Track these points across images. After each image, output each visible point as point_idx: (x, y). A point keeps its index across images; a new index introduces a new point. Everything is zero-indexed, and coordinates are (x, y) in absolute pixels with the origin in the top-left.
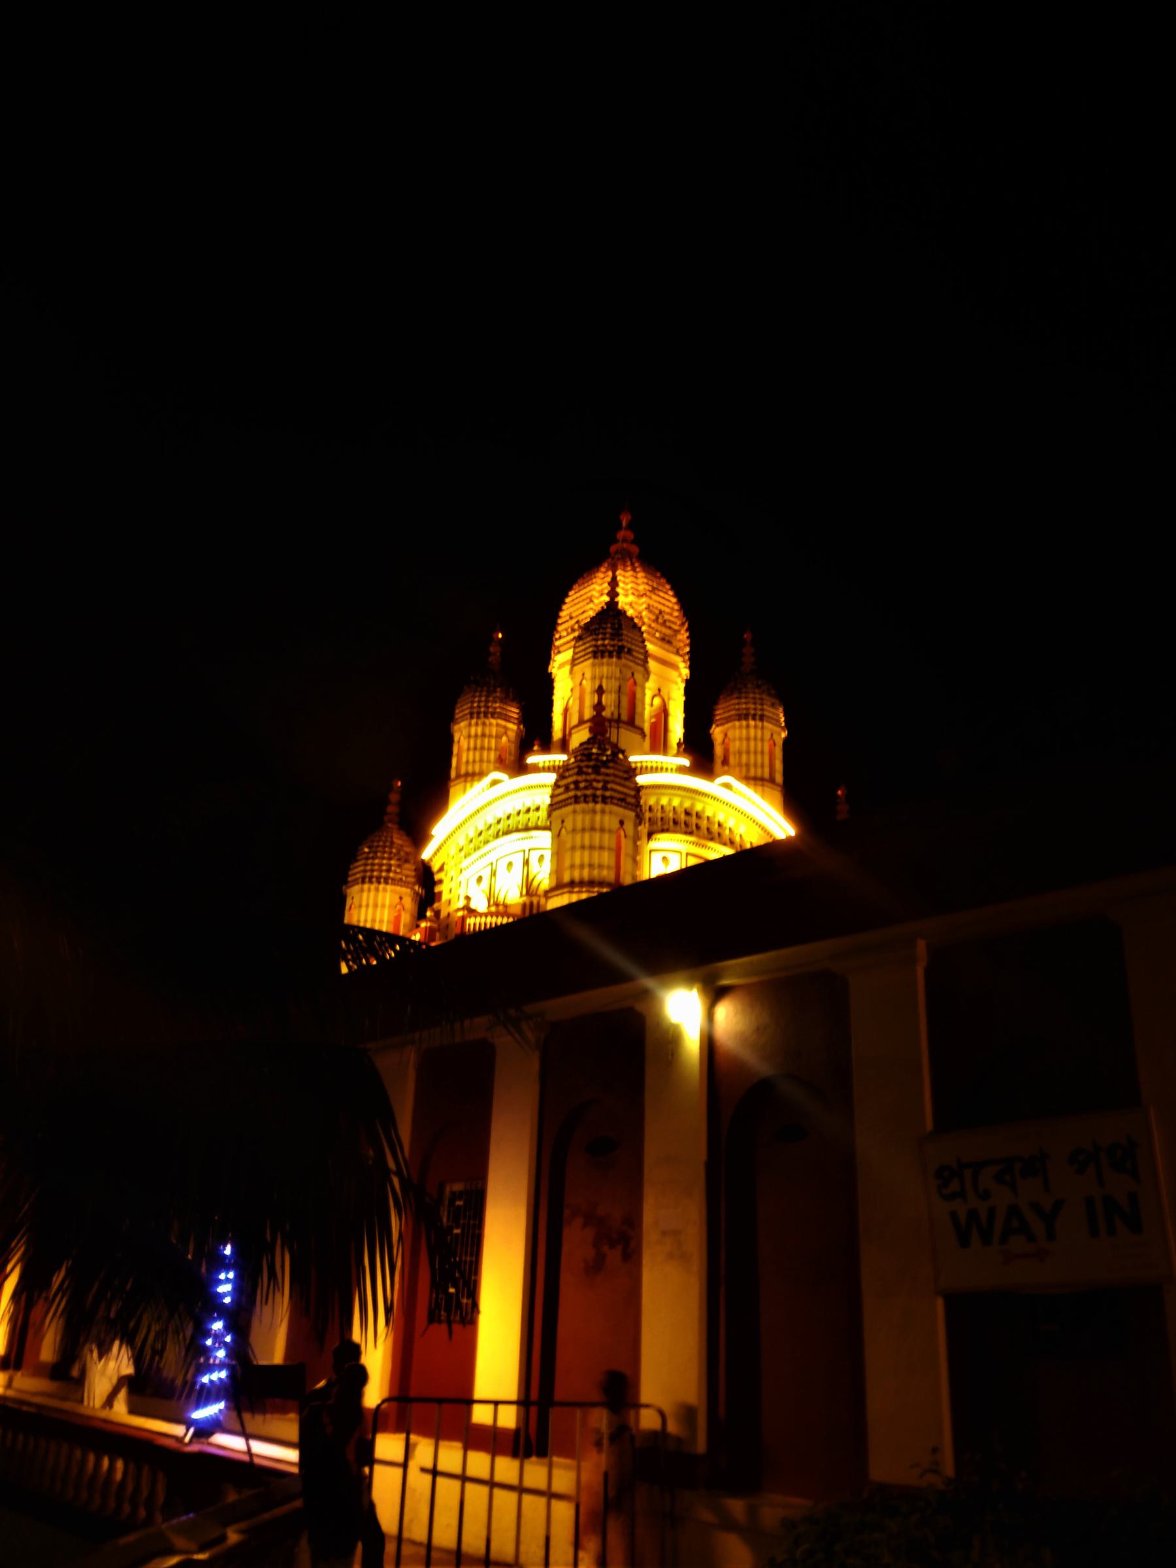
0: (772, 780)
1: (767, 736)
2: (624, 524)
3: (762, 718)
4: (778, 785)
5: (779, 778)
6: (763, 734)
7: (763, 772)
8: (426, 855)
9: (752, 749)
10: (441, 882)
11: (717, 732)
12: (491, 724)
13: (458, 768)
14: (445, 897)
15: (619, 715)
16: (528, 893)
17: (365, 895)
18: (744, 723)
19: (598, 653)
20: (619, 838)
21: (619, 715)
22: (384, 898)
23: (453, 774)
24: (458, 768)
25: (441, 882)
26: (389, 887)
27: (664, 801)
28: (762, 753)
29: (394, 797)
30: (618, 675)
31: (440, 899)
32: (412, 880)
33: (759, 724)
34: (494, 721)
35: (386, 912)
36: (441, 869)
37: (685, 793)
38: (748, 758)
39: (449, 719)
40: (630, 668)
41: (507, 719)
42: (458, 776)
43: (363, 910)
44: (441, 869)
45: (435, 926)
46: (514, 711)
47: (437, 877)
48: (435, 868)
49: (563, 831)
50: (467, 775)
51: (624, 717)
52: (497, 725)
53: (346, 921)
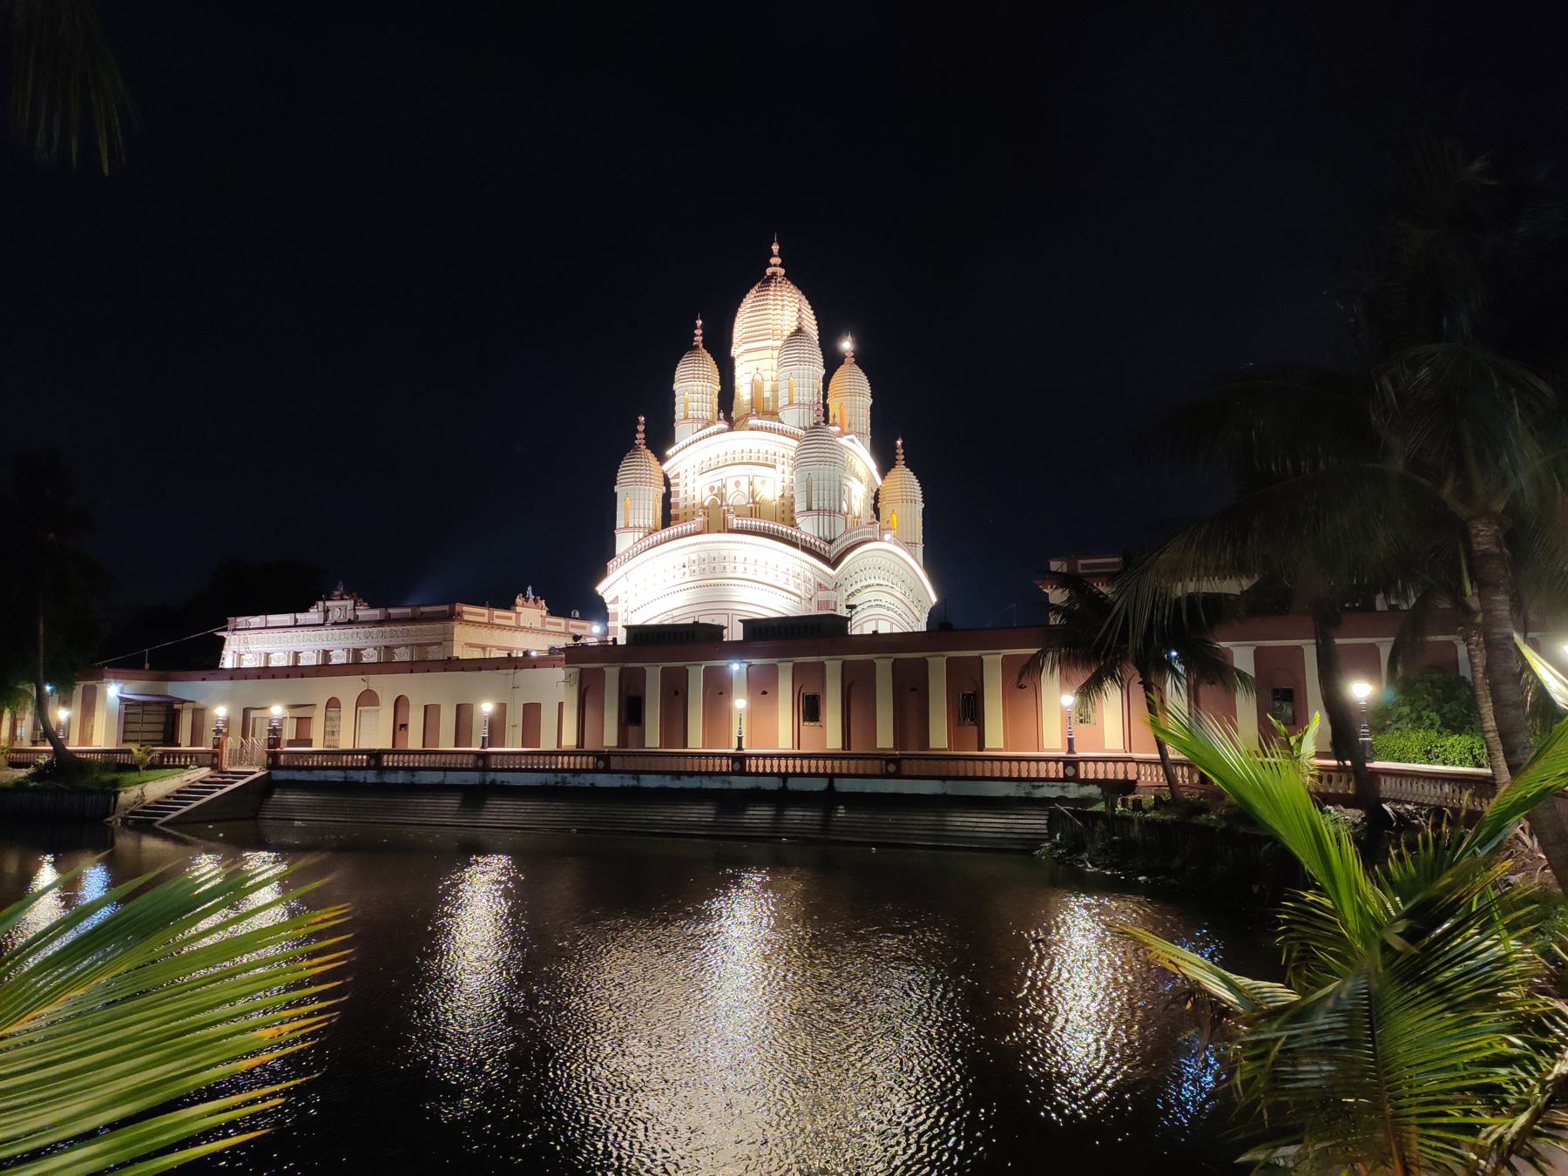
14: (682, 495)
53: (600, 589)
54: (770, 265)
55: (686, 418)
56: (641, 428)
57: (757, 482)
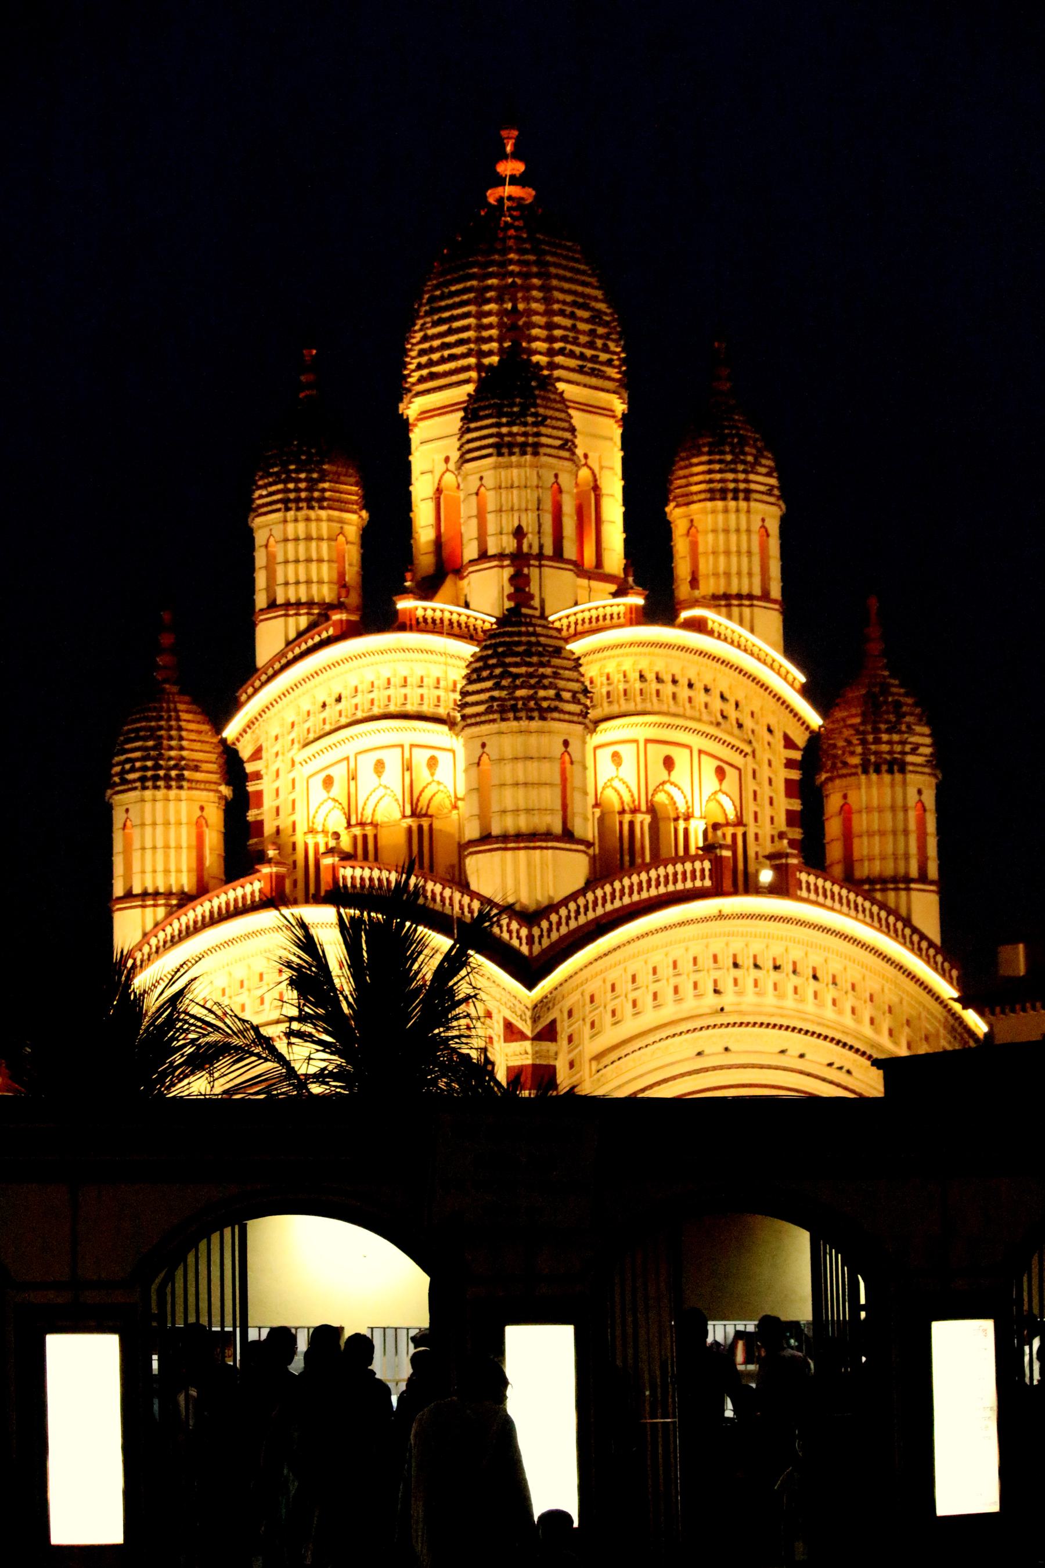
0: (765, 596)
1: (756, 525)
2: (509, 149)
3: (748, 495)
4: (775, 602)
5: (776, 592)
6: (748, 522)
7: (751, 584)
8: (230, 732)
9: (734, 548)
10: (257, 776)
11: (676, 514)
12: (319, 520)
13: (270, 589)
15: (541, 547)
16: (414, 814)
17: (148, 806)
18: (720, 504)
19: (502, 448)
20: (563, 763)
21: (541, 547)
22: (178, 812)
23: (261, 600)
24: (270, 589)
25: (257, 776)
26: (183, 794)
27: (611, 667)
28: (749, 553)
29: (166, 640)
30: (535, 481)
31: (259, 805)
32: (214, 777)
33: (743, 504)
34: (323, 514)
35: (184, 830)
36: (257, 755)
37: (640, 649)
38: (728, 564)
39: (246, 508)
40: (551, 467)
41: (341, 505)
42: (272, 605)
43: (148, 830)
44: (257, 755)
45: (282, 870)
46: (351, 491)
47: (249, 768)
48: (245, 753)
49: (485, 758)
50: (288, 605)
51: (549, 551)
52: (330, 519)
54: (500, 181)
55: (272, 605)
56: (166, 640)
57: (420, 758)
